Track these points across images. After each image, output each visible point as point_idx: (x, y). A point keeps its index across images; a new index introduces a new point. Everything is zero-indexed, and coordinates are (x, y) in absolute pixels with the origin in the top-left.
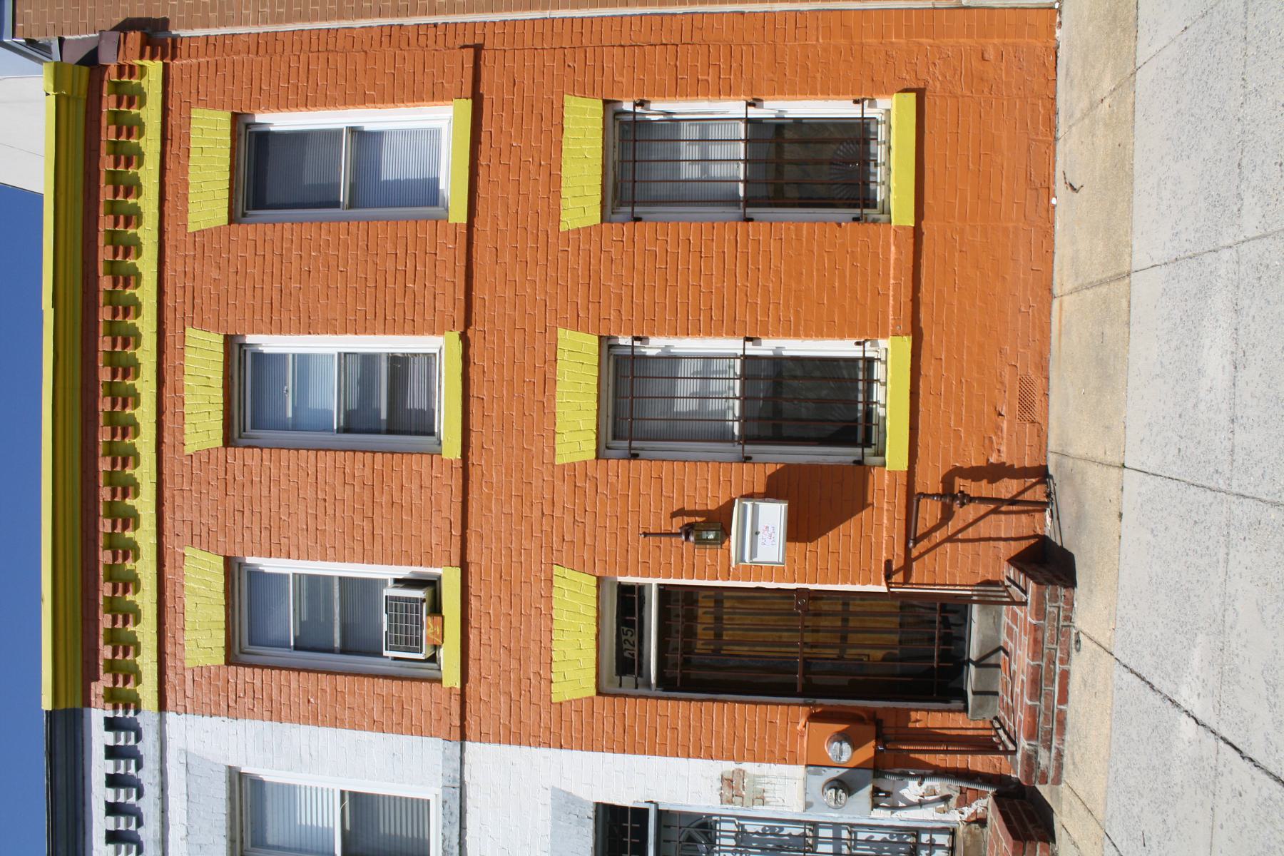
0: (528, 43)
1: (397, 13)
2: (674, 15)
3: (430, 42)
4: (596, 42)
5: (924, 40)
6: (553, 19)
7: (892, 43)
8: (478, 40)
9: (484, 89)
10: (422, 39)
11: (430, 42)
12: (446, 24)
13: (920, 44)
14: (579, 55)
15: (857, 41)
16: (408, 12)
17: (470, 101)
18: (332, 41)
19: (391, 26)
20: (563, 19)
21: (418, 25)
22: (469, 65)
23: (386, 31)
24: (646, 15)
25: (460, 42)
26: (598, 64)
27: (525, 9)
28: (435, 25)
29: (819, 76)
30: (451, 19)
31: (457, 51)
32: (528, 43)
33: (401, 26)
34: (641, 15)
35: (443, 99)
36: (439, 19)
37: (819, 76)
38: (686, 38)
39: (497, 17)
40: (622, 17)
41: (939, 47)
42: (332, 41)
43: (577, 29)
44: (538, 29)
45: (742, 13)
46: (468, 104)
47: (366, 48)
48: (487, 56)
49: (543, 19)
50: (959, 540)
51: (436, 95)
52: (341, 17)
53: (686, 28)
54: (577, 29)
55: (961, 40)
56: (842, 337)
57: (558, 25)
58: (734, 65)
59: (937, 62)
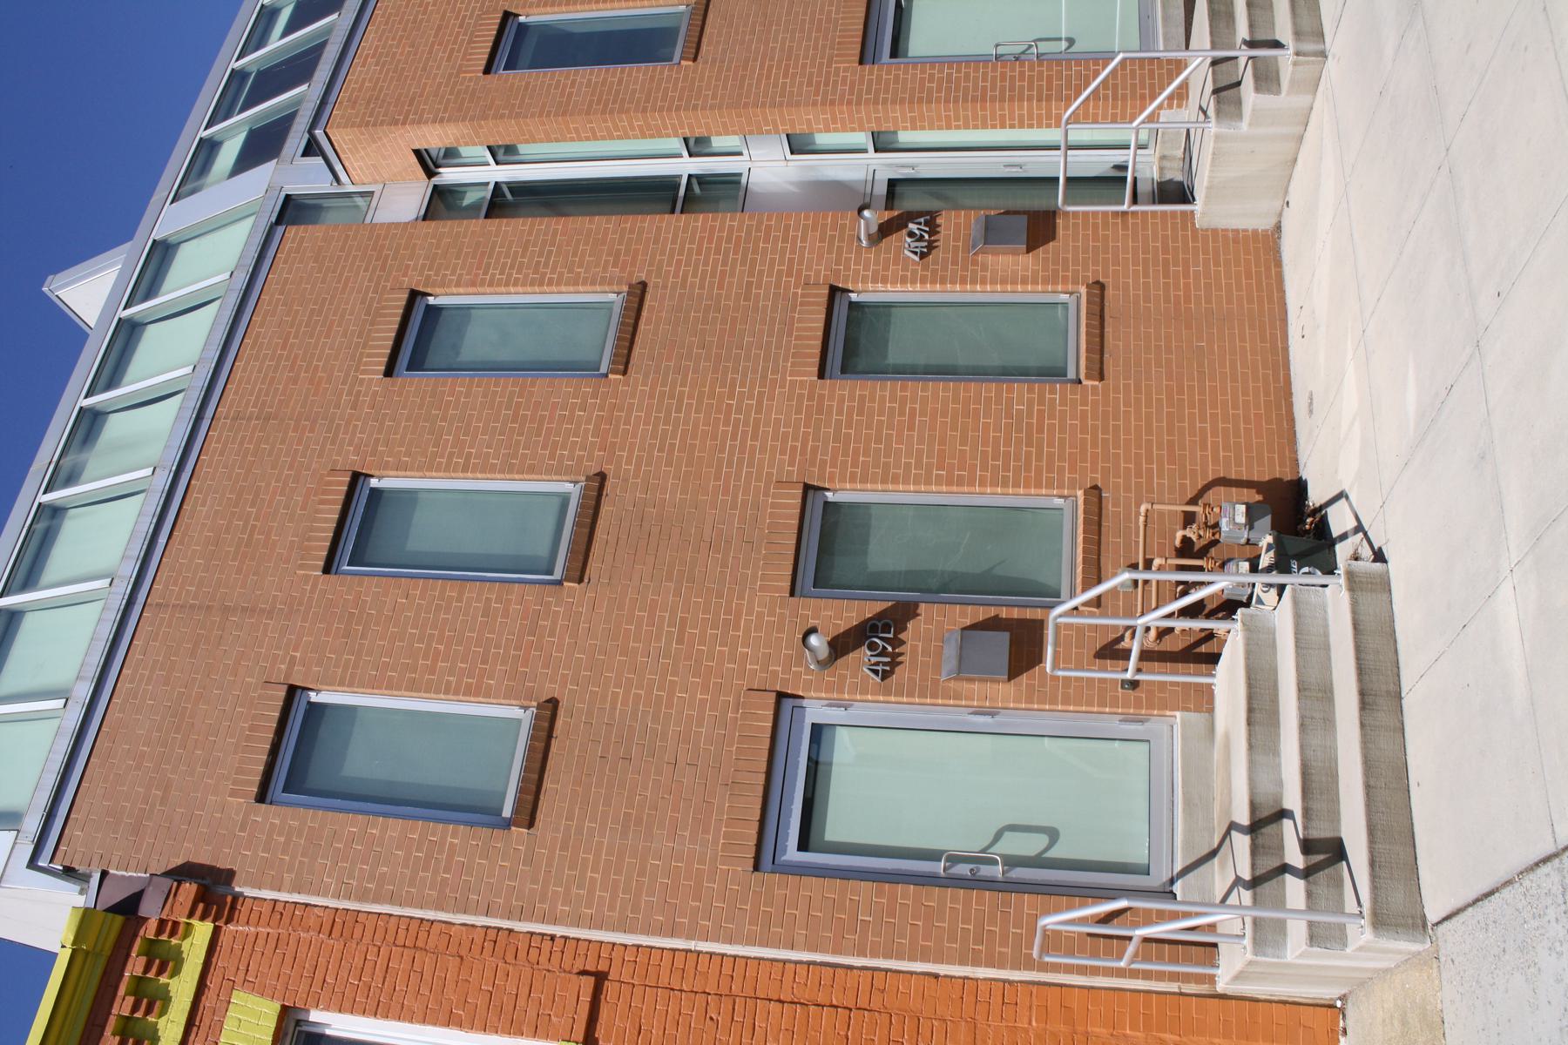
2: (851, 968)
6: (699, 953)
8: (602, 967)
14: (726, 1004)
15: (1080, 1029)
18: (422, 935)
22: (586, 998)
25: (579, 966)
26: (748, 1021)
28: (553, 938)
30: (573, 932)
33: (510, 931)
34: (809, 963)
36: (559, 931)
43: (726, 970)
45: (936, 976)
48: (610, 988)
54: (726, 970)
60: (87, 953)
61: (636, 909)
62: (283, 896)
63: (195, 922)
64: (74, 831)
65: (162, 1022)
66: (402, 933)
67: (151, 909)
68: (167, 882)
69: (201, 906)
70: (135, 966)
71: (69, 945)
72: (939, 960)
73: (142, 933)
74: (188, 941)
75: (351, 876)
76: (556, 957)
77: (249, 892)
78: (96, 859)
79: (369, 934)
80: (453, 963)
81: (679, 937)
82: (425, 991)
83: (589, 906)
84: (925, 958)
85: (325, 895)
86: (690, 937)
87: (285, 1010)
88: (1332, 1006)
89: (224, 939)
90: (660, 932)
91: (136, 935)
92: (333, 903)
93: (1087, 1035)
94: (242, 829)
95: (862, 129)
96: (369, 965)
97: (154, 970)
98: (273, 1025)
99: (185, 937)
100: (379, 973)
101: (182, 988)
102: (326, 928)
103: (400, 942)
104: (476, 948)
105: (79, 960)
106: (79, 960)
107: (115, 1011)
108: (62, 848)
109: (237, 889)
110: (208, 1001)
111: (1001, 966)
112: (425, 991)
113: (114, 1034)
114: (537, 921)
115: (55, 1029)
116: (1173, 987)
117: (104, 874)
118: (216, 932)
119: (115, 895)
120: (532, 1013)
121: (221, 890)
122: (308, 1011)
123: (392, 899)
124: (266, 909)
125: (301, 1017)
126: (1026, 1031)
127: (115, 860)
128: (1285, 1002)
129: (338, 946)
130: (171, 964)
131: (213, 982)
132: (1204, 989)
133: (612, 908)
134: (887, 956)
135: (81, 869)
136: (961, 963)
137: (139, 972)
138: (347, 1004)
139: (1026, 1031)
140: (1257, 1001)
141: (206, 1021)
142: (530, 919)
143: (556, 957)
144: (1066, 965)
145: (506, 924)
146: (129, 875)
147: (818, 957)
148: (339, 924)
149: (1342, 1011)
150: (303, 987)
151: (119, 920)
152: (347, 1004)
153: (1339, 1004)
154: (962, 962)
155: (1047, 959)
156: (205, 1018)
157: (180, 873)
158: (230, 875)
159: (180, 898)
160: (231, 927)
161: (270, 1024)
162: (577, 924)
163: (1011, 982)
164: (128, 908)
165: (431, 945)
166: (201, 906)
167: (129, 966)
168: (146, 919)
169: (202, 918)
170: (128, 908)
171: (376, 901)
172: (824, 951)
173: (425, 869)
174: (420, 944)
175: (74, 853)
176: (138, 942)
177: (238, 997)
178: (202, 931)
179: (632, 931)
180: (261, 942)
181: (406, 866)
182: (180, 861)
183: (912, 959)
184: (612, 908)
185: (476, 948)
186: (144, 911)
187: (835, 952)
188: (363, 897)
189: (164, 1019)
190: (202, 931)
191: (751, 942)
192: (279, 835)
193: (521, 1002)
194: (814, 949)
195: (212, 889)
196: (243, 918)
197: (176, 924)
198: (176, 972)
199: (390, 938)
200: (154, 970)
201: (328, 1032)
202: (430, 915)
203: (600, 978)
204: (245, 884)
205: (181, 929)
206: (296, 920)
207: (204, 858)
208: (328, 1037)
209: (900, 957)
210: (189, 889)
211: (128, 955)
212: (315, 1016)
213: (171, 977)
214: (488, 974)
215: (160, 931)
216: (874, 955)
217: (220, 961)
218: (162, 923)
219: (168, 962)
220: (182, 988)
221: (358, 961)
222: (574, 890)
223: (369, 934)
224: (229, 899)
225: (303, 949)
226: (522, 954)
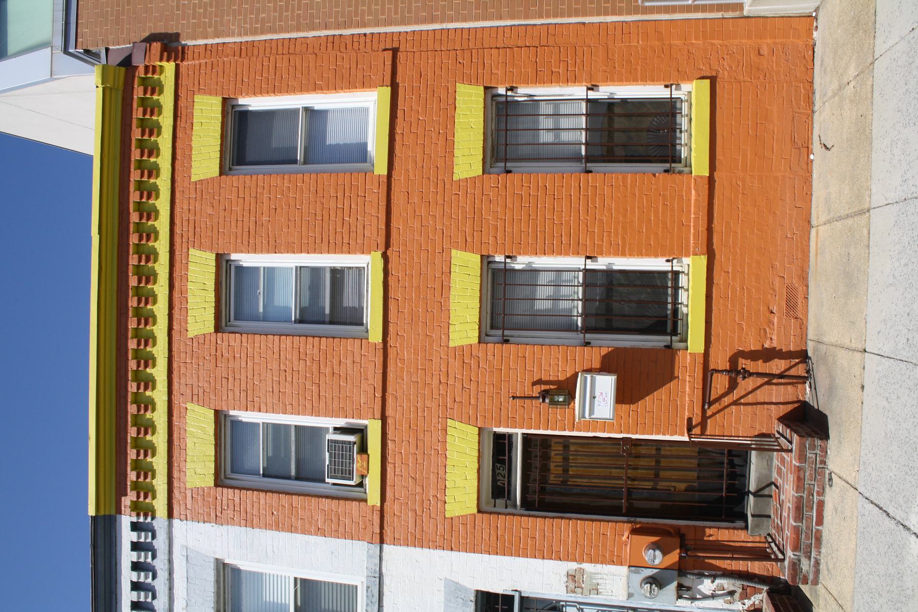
0: (431, 47)
1: (338, 27)
2: (535, 25)
5: (716, 42)
6: (448, 30)
7: (692, 44)
8: (395, 45)
9: (399, 79)
10: (356, 44)
13: (713, 44)
14: (467, 54)
15: (667, 42)
16: (345, 26)
17: (389, 88)
18: (292, 47)
22: (389, 63)
23: (330, 40)
25: (382, 47)
26: (480, 61)
28: (365, 35)
29: (639, 68)
30: (376, 30)
31: (380, 53)
32: (431, 47)
33: (341, 35)
34: (511, 26)
35: (370, 87)
36: (368, 31)
37: (639, 68)
38: (544, 42)
39: (409, 28)
40: (497, 27)
41: (726, 46)
43: (465, 36)
45: (584, 24)
48: (401, 56)
51: (365, 84)
52: (299, 30)
53: (544, 35)
54: (465, 36)
55: (743, 41)
59: (725, 57)
60: (111, 89)
61: (409, 12)
62: (210, 41)
63: (164, 64)
64: (83, 30)
65: (160, 119)
66: (280, 47)
67: (139, 61)
68: (144, 44)
69: (165, 54)
70: (138, 92)
71: (100, 86)
72: (585, 15)
73: (137, 74)
74: (163, 75)
75: (245, 23)
76: (369, 45)
77: (190, 43)
78: (100, 43)
79: (262, 52)
80: (312, 58)
81: (436, 22)
82: (299, 75)
83: (383, 14)
84: (577, 15)
85: (233, 35)
86: (442, 22)
87: (225, 100)
88: (811, 16)
89: (183, 70)
90: (425, 21)
91: (134, 77)
92: (238, 40)
93: (670, 46)
94: (178, 9)
95: (477, 84)
96: (265, 68)
97: (149, 92)
98: (220, 108)
99: (161, 73)
100: (272, 70)
101: (166, 100)
102: (237, 53)
103: (280, 52)
104: (323, 48)
105: (108, 93)
106: (108, 93)
107: (135, 97)
108: (80, 40)
109: (183, 42)
110: (182, 103)
111: (621, 14)
112: (299, 75)
113: (132, 470)
114: (355, 27)
115: (106, 152)
116: (719, 15)
117: (107, 50)
118: (177, 67)
119: (115, 59)
120: (360, 75)
121: (174, 45)
122: (237, 99)
123: (272, 30)
124: (202, 51)
125: (234, 103)
126: (637, 47)
127: (111, 37)
128: (783, 17)
129: (246, 61)
130: (157, 88)
131: (182, 93)
132: (737, 14)
133: (396, 13)
134: (555, 16)
135: (94, 49)
136: (597, 15)
137: (135, 305)
138: (257, 90)
139: (637, 47)
140: (767, 17)
141: (184, 113)
142: (350, 27)
143: (369, 45)
144: (658, 7)
145: (337, 32)
146: (120, 47)
147: (516, 22)
148: (243, 50)
149: (816, 18)
150: (232, 86)
151: (123, 69)
152: (257, 90)
153: (814, 14)
154: (599, 14)
155: (647, 4)
156: (183, 111)
157: (151, 39)
158: (176, 37)
159: (153, 52)
160: (185, 63)
161: (218, 108)
162: (377, 24)
163: (626, 22)
164: (127, 63)
165: (298, 50)
166: (165, 54)
167: (132, 156)
168: (137, 67)
169: (168, 61)
170: (127, 63)
171: (262, 33)
172: (519, 18)
173: (287, 11)
174: (291, 51)
175: (89, 37)
176: (136, 80)
177: (198, 98)
178: (169, 67)
179: (409, 24)
180: (203, 67)
181: (275, 11)
182: (147, 34)
183: (570, 16)
184: (396, 13)
185: (323, 48)
186: (135, 62)
187: (526, 17)
188: (254, 32)
189: (161, 116)
190: (169, 67)
191: (477, 19)
192: (200, 8)
193: (353, 71)
194: (513, 18)
195: (170, 45)
196: (190, 57)
197: (154, 67)
198: (161, 92)
199: (274, 51)
200: (149, 92)
201: (250, 109)
202: (294, 35)
203: (395, 51)
204: (187, 39)
205: (158, 69)
206: (220, 52)
207: (160, 29)
208: (251, 111)
209: (562, 16)
210: (156, 46)
211: (133, 88)
212: (241, 101)
213: (159, 95)
214: (333, 60)
215: (146, 72)
216: (548, 16)
217: (183, 82)
218: (147, 67)
219: (157, 88)
220: (166, 100)
221: (259, 67)
222: (373, 7)
223: (262, 52)
224: (180, 48)
225: (227, 66)
226: (349, 46)
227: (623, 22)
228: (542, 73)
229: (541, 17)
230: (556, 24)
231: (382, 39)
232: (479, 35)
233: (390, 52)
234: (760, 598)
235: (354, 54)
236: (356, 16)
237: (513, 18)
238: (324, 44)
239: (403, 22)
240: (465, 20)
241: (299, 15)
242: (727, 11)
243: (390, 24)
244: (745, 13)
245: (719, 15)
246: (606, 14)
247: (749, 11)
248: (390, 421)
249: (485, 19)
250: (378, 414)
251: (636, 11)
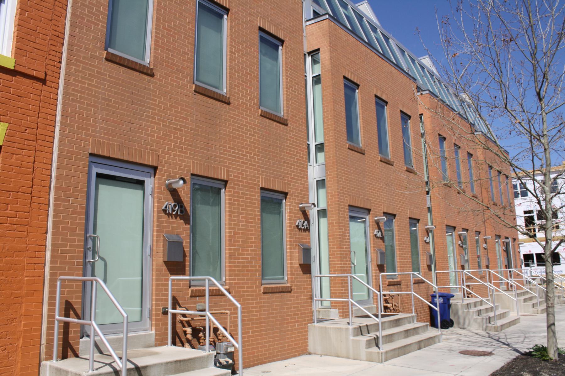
0: (42, 110)
1: (70, 44)
2: (49, 194)
3: (51, 57)
4: (39, 148)
5: (21, 341)
6: (55, 127)
7: (21, 321)
8: (48, 83)
9: (18, 78)
10: (54, 53)
11: (51, 57)
12: (60, 68)
13: (18, 339)
14: (32, 137)
15: (24, 300)
16: (70, 50)
17: (13, 68)
18: (61, 5)
19: (64, 39)
20: (54, 132)
21: (62, 53)
22: (35, 74)
23: (61, 35)
24: (51, 178)
25: (49, 73)
26: (25, 147)
27: (62, 112)
28: (60, 62)
29: (4, 277)
30: (63, 72)
31: (44, 69)
32: (42, 110)
33: (63, 44)
34: (51, 176)
35: (16, 53)
36: (63, 65)
37: (4, 277)
38: (34, 199)
39: (60, 96)
40: (51, 165)
41: (16, 351)
42: (61, 5)
43: (47, 138)
44: (50, 117)
45: (46, 233)
46: (11, 65)
47: (53, 21)
48: (39, 85)
49: (55, 121)
50: (534, 183)
51: (19, 50)
52: (73, 14)
53: (41, 200)
54: (47, 138)
55: (19, 365)
56: (324, 135)
57: (51, 128)
58: (15, 226)
59: (6, 351)
72: (54, 234)
84: (54, 228)
86: (61, 123)
90: (64, 110)
93: (21, 303)
111: (52, 262)
116: (44, 341)
126: (22, 275)
132: (43, 355)
133: (73, 90)
134: (55, 211)
139: (22, 275)
154: (53, 245)
162: (67, 74)
163: (44, 267)
172: (57, 182)
179: (64, 98)
183: (54, 222)
184: (73, 90)
187: (56, 188)
191: (60, 150)
193: (32, 44)
209: (54, 216)
214: (44, 31)
216: (55, 205)
222: (81, 75)
226: (53, 48)
227: (45, 264)
228: (8, 195)
229: (56, 199)
230: (48, 210)
231: (55, 74)
232: (47, 149)
233: (43, 78)
234: (560, 373)
235: (46, 50)
236: (76, 60)
237: (57, 178)
238: (58, 29)
239: (65, 94)
240: (60, 141)
241: (84, 19)
242: (47, 347)
243: (66, 83)
244: (43, 363)
245: (44, 341)
246: (53, 251)
247: (46, 366)
248: (8, 77)
249: (59, 156)
250: (19, 69)
251: (53, 275)
